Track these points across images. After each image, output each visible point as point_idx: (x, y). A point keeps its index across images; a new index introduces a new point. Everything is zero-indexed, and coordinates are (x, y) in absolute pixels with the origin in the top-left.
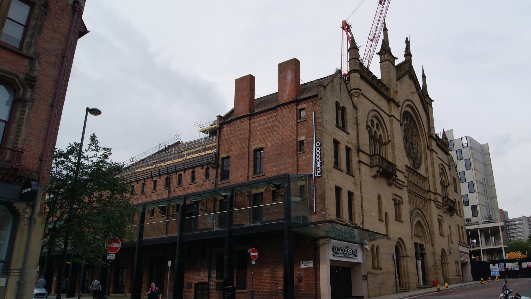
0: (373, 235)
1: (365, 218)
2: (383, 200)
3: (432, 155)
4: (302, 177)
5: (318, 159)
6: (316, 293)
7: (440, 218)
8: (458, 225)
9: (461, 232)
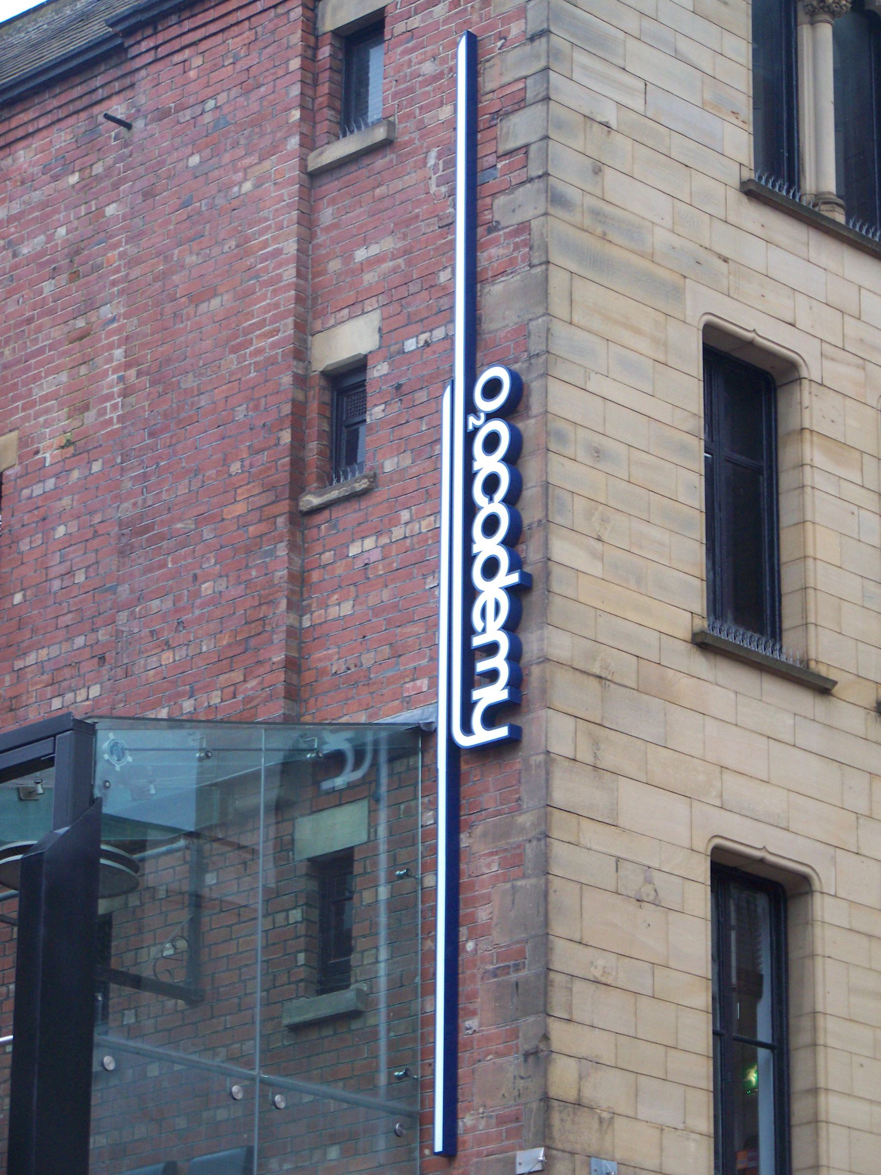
4: (336, 761)
5: (487, 547)
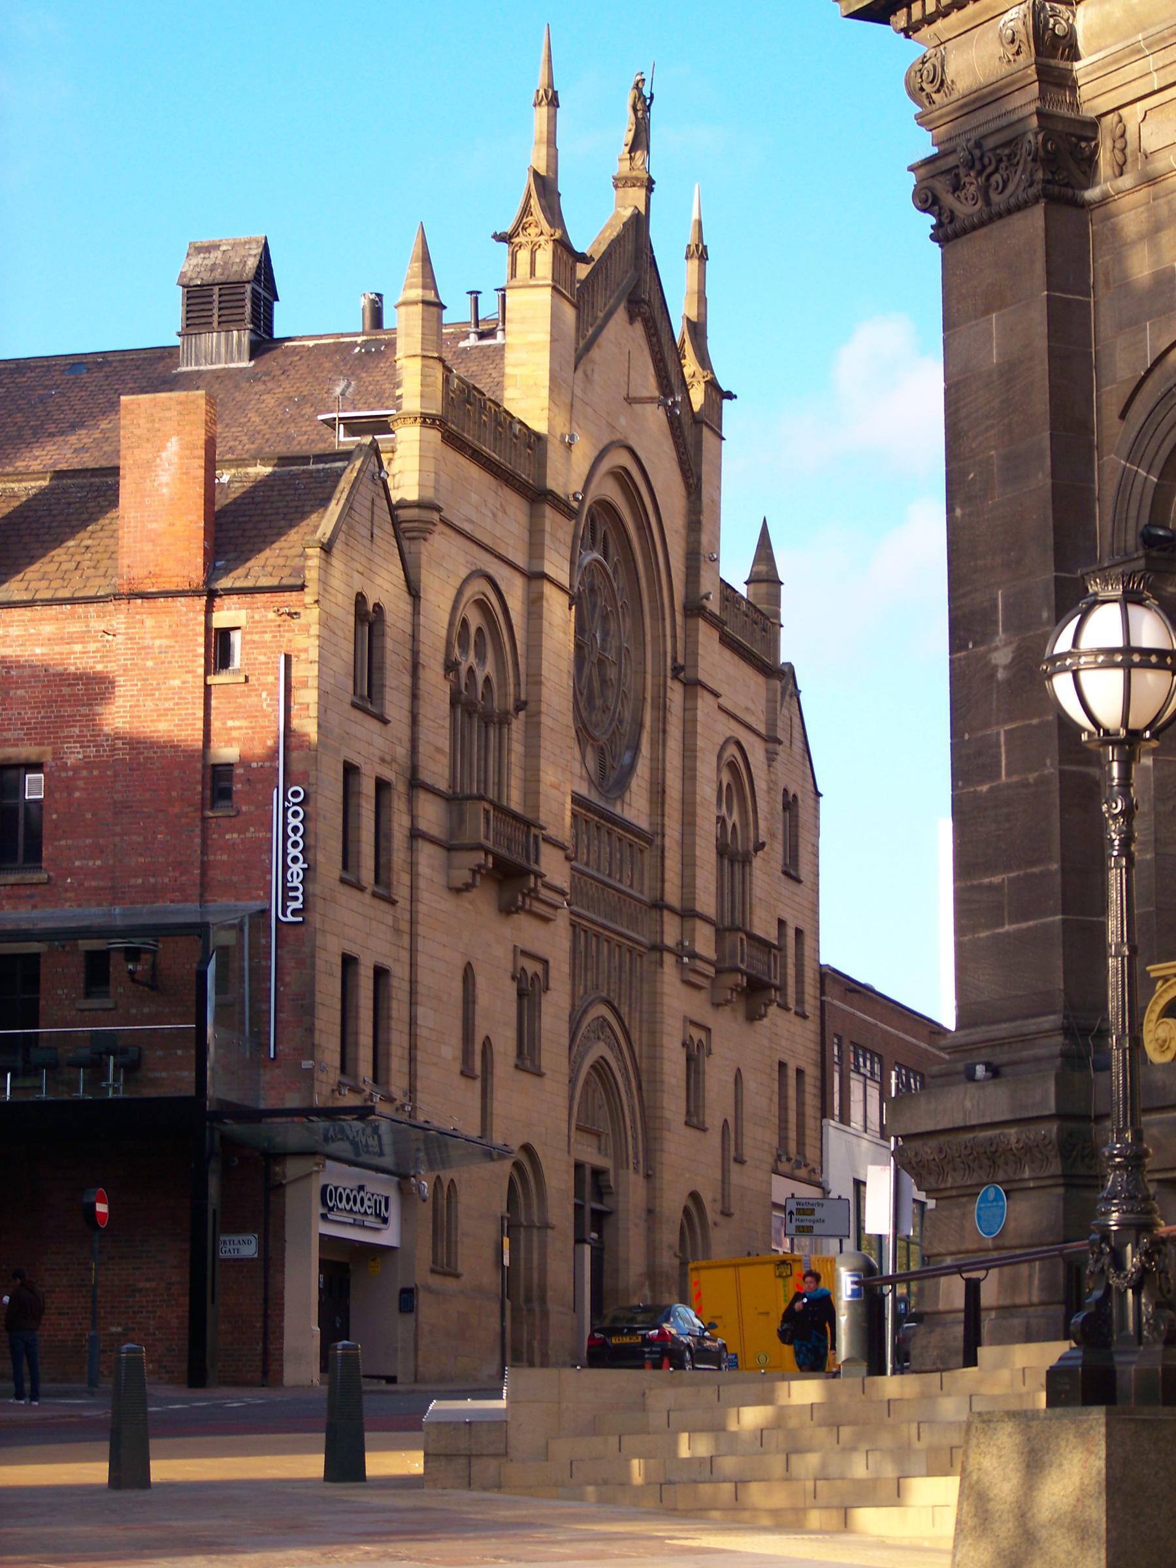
0: (438, 1144)
1: (421, 1070)
2: (481, 981)
3: (689, 712)
6: (266, 1352)
7: (698, 1035)
8: (782, 1065)
9: (792, 1104)
